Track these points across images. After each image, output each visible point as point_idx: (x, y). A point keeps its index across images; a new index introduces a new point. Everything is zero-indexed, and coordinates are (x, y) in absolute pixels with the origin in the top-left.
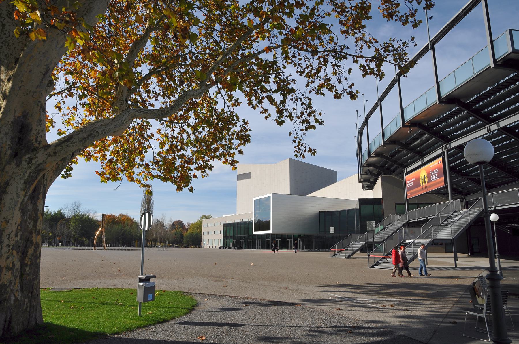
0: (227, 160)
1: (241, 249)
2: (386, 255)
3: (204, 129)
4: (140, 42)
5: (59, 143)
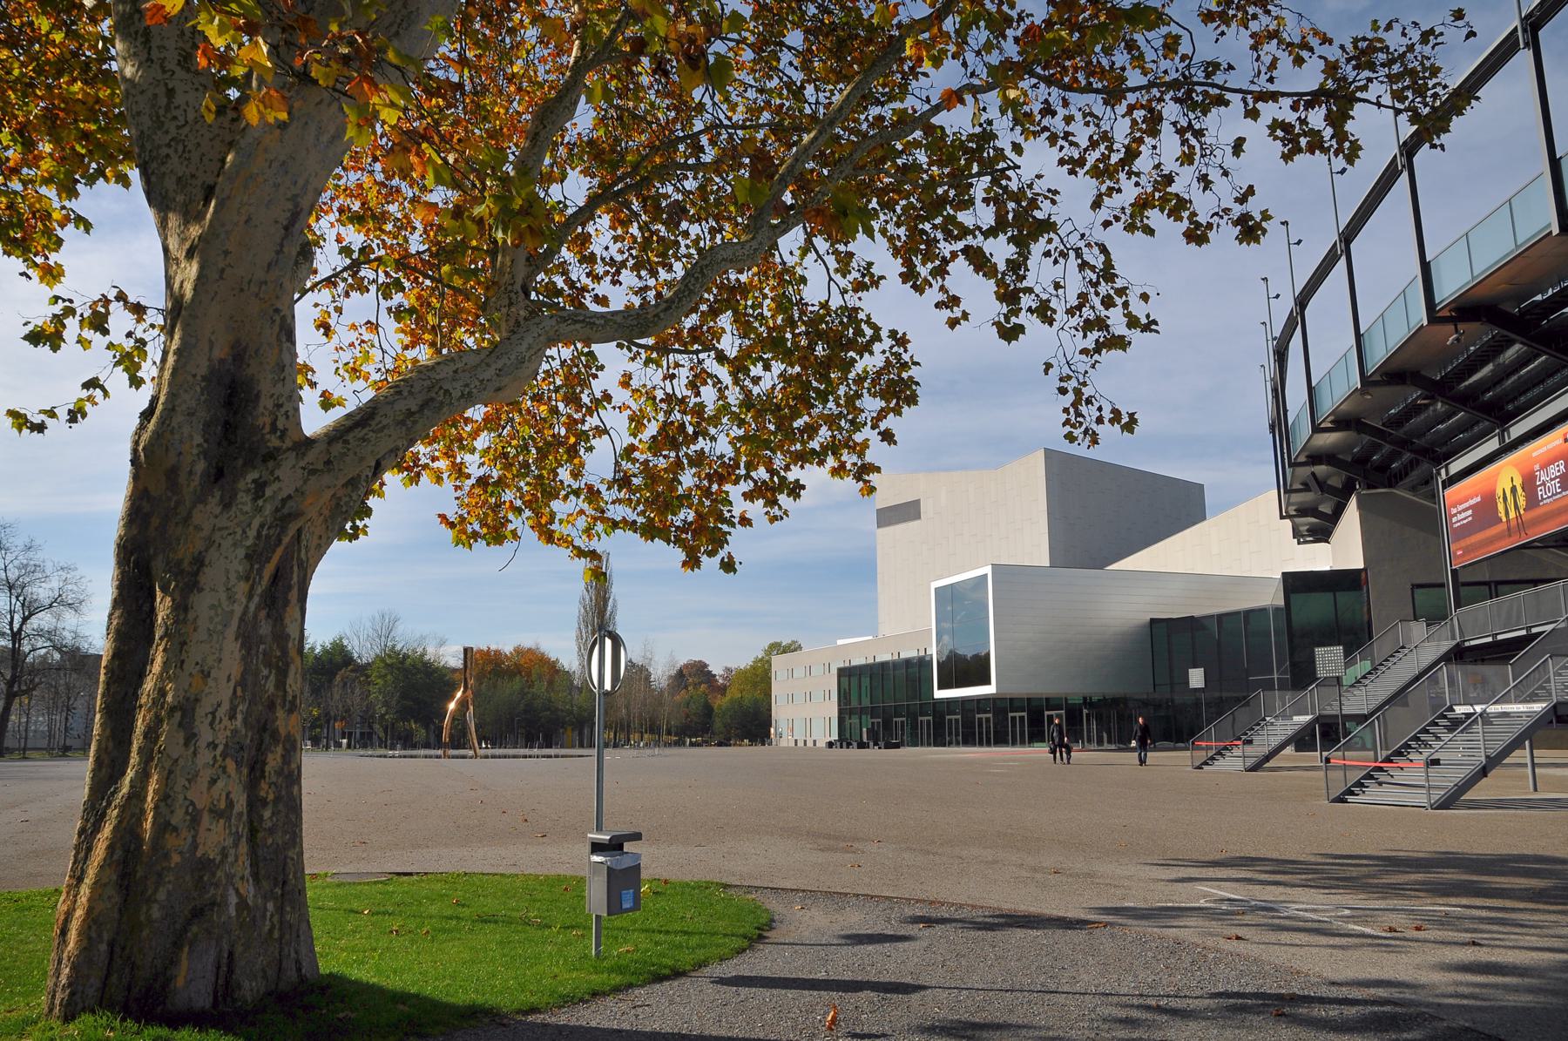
0: (842, 465)
1: (897, 746)
2: (1388, 760)
3: (767, 368)
4: (555, 109)
5: (338, 434)
